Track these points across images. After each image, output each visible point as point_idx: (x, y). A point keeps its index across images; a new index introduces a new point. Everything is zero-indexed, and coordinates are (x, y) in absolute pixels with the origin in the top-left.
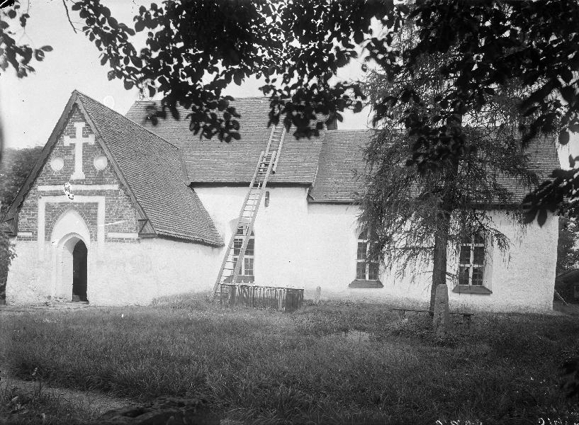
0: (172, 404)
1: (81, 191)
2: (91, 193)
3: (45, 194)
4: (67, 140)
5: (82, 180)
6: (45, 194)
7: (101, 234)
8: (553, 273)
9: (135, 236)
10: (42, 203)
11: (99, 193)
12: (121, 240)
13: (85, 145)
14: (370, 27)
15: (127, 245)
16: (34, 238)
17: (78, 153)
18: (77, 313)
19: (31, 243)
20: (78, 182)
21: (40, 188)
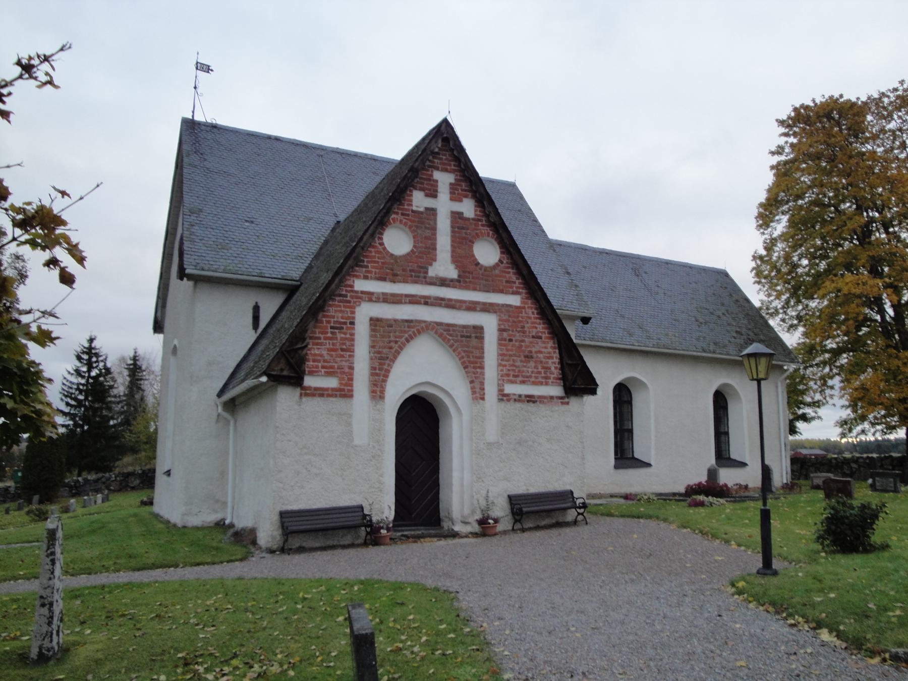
0: (834, 662)
1: (450, 300)
2: (472, 307)
3: (370, 297)
4: (419, 200)
5: (452, 280)
6: (370, 297)
7: (491, 390)
8: (758, 561)
9: (556, 390)
10: (364, 312)
11: (487, 308)
12: (530, 399)
13: (457, 217)
14: (774, 171)
15: (542, 410)
16: (345, 392)
17: (444, 225)
18: (553, 338)
19: (337, 404)
20: (443, 282)
21: (360, 285)
